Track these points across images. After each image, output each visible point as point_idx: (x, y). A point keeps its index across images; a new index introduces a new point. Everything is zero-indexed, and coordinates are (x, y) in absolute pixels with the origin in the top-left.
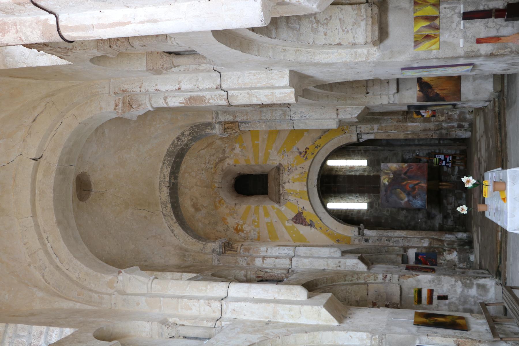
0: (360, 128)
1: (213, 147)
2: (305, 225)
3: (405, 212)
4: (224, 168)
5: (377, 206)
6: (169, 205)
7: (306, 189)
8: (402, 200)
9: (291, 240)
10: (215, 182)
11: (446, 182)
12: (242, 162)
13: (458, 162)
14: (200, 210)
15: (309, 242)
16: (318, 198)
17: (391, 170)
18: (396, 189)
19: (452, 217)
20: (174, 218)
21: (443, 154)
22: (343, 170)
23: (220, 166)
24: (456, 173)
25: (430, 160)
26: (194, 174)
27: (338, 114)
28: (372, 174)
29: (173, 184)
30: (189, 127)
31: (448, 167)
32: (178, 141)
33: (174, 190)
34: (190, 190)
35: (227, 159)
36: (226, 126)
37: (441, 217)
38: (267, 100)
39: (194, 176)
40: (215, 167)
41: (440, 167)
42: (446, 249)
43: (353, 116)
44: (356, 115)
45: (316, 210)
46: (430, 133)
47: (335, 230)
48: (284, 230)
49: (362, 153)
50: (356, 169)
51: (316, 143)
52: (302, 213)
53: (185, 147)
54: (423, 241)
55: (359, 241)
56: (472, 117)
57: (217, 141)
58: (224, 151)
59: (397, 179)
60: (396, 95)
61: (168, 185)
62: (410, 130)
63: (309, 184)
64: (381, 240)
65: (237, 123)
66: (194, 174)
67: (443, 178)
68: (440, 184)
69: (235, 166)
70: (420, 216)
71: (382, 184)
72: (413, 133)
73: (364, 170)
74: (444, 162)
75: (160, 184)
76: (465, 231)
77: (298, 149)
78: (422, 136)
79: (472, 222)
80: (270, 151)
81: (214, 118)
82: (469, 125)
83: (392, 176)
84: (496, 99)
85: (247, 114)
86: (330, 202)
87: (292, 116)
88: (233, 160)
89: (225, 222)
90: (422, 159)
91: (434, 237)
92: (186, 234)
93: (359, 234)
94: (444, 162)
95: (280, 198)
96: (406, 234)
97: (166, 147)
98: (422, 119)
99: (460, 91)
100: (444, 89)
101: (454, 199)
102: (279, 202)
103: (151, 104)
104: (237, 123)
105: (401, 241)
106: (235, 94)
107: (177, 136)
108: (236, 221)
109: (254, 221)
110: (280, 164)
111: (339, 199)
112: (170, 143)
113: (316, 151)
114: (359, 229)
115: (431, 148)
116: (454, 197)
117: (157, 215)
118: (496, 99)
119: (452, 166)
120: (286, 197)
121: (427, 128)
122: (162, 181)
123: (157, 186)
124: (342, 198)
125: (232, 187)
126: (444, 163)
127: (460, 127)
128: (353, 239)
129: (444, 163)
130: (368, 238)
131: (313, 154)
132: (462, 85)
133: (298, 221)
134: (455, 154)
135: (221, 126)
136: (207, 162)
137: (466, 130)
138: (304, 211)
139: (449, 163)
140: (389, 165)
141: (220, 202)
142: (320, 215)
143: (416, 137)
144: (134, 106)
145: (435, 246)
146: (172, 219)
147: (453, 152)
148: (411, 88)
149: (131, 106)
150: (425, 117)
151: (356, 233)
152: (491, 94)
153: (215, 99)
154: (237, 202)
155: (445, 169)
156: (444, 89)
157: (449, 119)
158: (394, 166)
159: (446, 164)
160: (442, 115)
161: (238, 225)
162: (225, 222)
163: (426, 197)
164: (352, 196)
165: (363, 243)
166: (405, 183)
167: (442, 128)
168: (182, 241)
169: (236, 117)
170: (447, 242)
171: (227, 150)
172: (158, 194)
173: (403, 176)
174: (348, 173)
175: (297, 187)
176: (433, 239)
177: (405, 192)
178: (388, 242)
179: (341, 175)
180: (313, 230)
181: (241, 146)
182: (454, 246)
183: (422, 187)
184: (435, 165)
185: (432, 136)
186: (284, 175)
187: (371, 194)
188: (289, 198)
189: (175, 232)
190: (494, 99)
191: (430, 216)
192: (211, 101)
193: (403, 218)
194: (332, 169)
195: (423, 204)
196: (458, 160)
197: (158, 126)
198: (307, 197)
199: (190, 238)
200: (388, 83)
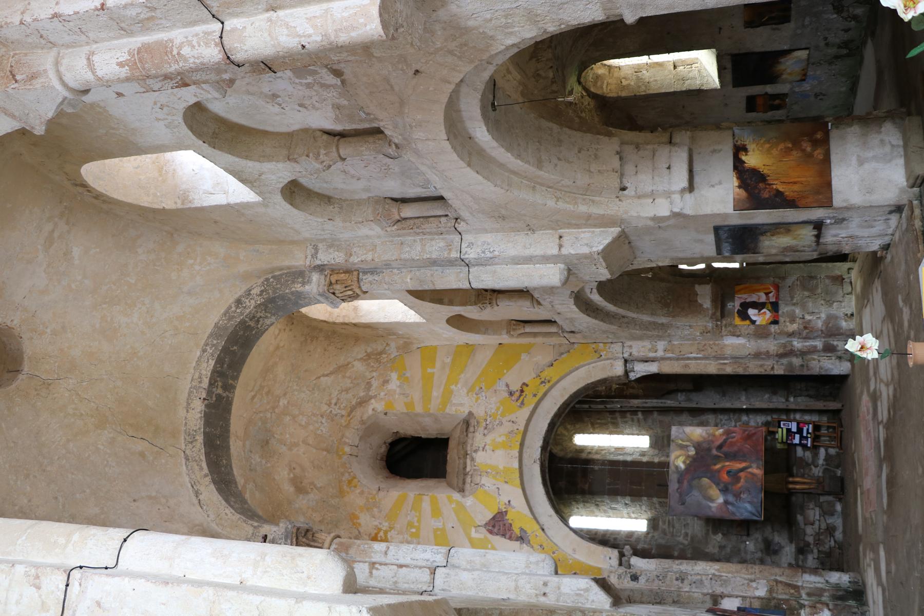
0: (631, 347)
1: (348, 374)
2: (510, 538)
4: (365, 417)
5: (666, 527)
6: (200, 438)
7: (516, 465)
8: (712, 501)
10: (345, 443)
11: (803, 476)
12: (400, 407)
14: (307, 493)
16: (541, 486)
17: (690, 440)
18: (700, 478)
19: (815, 551)
20: (204, 465)
23: (358, 413)
24: (821, 462)
26: (303, 420)
27: (560, 246)
29: (219, 397)
30: (262, 280)
31: (805, 447)
32: (237, 307)
33: (217, 412)
34: (290, 449)
35: (373, 401)
36: (334, 279)
37: (793, 550)
38: (311, 31)
39: (303, 423)
40: (349, 415)
42: (806, 603)
43: (595, 249)
44: (601, 247)
46: (769, 363)
47: (570, 551)
49: (638, 420)
51: (543, 375)
52: (506, 512)
53: (252, 324)
54: (754, 585)
55: (620, 577)
56: (852, 327)
57: (356, 363)
58: (369, 385)
59: (703, 459)
60: (687, 196)
61: (204, 395)
63: (525, 456)
64: (665, 577)
65: (355, 273)
66: (303, 420)
68: (791, 479)
69: (386, 414)
71: (672, 468)
72: (736, 359)
73: (643, 454)
74: (797, 436)
75: (190, 393)
77: (507, 385)
78: (754, 368)
80: (453, 387)
81: (309, 257)
83: (692, 452)
84: (915, 202)
85: (374, 248)
86: (576, 514)
87: (463, 251)
88: (383, 403)
89: (354, 524)
91: (779, 579)
92: (223, 502)
93: (620, 564)
94: (797, 436)
95: (464, 483)
96: (718, 570)
97: (214, 317)
98: (752, 327)
99: (829, 185)
100: (795, 183)
101: (817, 513)
102: (462, 490)
103: (58, 71)
104: (355, 273)
105: (707, 583)
106: (238, 26)
107: (236, 296)
108: (376, 523)
109: (410, 525)
110: (470, 413)
111: (593, 508)
112: (222, 311)
114: (622, 555)
116: (817, 509)
117: (171, 456)
118: (915, 202)
120: (477, 479)
121: (763, 350)
122: (195, 387)
123: (183, 397)
124: (597, 505)
125: (382, 459)
126: (797, 440)
129: (797, 440)
131: (535, 395)
132: (833, 174)
133: (495, 530)
135: (323, 277)
136: (334, 401)
138: (509, 509)
139: (807, 438)
140: (688, 429)
141: (350, 482)
142: (543, 520)
144: (18, 77)
145: (780, 597)
146: (201, 469)
148: (720, 183)
149: (14, 76)
150: (757, 323)
151: (615, 562)
152: (902, 191)
153: (195, 43)
154: (382, 486)
155: (799, 451)
156: (795, 183)
157: (805, 328)
158: (697, 432)
159: (801, 440)
160: (793, 321)
161: (380, 530)
162: (354, 524)
164: (618, 502)
166: (718, 466)
168: (212, 517)
169: (351, 255)
170: (808, 590)
171: (375, 384)
172: (182, 413)
173: (714, 452)
174: (612, 457)
175: (502, 466)
176: (777, 581)
177: (717, 484)
178: (679, 582)
179: (598, 460)
181: (401, 376)
182: (824, 599)
183: (753, 474)
184: (779, 446)
185: (773, 368)
186: (477, 434)
187: (655, 500)
188: (483, 482)
189: (201, 497)
190: (911, 202)
192: (186, 51)
193: (716, 550)
194: (581, 450)
197: (197, 268)
198: (518, 481)
199: (229, 511)
200: (669, 168)
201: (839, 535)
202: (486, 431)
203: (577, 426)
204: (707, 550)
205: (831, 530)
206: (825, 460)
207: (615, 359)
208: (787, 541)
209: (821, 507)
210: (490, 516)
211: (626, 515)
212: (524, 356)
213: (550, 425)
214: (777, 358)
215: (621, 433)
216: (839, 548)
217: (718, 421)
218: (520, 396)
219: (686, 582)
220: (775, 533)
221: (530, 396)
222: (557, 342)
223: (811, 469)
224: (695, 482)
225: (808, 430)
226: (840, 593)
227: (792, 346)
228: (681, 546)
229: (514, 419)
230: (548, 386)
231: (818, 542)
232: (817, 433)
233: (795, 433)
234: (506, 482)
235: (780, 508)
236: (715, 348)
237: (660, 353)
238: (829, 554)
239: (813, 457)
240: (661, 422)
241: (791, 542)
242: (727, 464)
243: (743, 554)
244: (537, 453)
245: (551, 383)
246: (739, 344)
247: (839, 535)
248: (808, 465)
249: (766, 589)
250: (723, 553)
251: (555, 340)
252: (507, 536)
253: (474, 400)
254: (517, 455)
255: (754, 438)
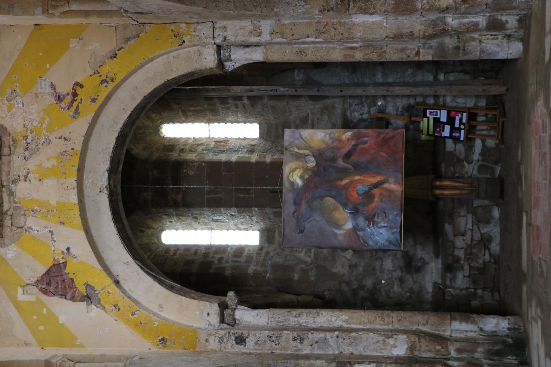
0: (224, 28)
2: (73, 299)
3: (349, 254)
7: (74, 198)
9: (32, 340)
11: (452, 178)
13: (482, 129)
15: (82, 346)
16: (112, 224)
17: (309, 148)
18: (322, 197)
19: (466, 267)
21: (444, 107)
22: (200, 148)
24: (476, 157)
25: (413, 122)
28: (268, 159)
31: (456, 140)
37: (440, 266)
41: (437, 141)
45: (105, 256)
47: (156, 310)
48: (13, 313)
49: (244, 106)
50: (231, 145)
51: (104, 71)
52: (65, 264)
54: (391, 341)
55: (221, 340)
59: (326, 172)
62: (359, 34)
63: (87, 183)
67: (443, 169)
68: (438, 183)
70: (388, 264)
71: (286, 184)
72: (368, 45)
73: (252, 149)
74: (447, 128)
76: (501, 311)
77: (53, 87)
78: (392, 54)
79: (524, 289)
82: (520, 21)
83: (312, 163)
86: (169, 228)
90: (393, 121)
93: (222, 321)
94: (447, 128)
101: (470, 221)
105: (332, 342)
111: (190, 221)
113: (105, 91)
114: (223, 307)
115: (415, 91)
116: (470, 216)
119: (467, 138)
120: (20, 221)
121: (406, 31)
124: (195, 218)
127: (495, 26)
128: (203, 337)
130: (245, 333)
133: (52, 289)
134: (475, 107)
137: (509, 37)
138: (69, 259)
139: (459, 129)
140: (306, 133)
142: (116, 269)
143: (375, 57)
145: (423, 355)
147: (470, 103)
151: (215, 319)
155: (450, 145)
158: (318, 137)
159: (451, 132)
163: (400, 219)
164: (221, 214)
165: (231, 346)
166: (345, 182)
167: (444, 32)
173: (341, 163)
174: (211, 157)
176: (420, 334)
177: (345, 205)
179: (193, 162)
180: (95, 310)
182: (477, 355)
183: (391, 192)
184: (424, 137)
185: (418, 53)
186: (14, 157)
187: (268, 210)
188: (29, 224)
191: (411, 265)
193: (345, 271)
194: (172, 145)
195: (392, 237)
196: (482, 123)
201: (495, 247)
202: (27, 153)
203: (165, 115)
204: (334, 270)
205: (485, 241)
206: (482, 154)
207: (204, 45)
208: (432, 255)
209: (474, 213)
210: (42, 270)
211: (234, 227)
212: (74, 44)
213: (118, 139)
214: (423, 41)
215: (223, 121)
216: (496, 263)
217: (347, 106)
218: (73, 101)
219: (306, 342)
220: (418, 247)
221: (87, 102)
222: (121, 23)
223: (463, 166)
224: (316, 203)
225: (461, 120)
226: (498, 347)
227: (445, 23)
228: (303, 266)
229: (67, 135)
230: (111, 86)
231: (470, 256)
232: (473, 123)
233: (444, 124)
234: (62, 223)
235: (424, 218)
236: (341, 29)
237: (265, 37)
238: (483, 270)
239: (466, 151)
240: (273, 107)
241: (437, 257)
242: (357, 178)
243: (378, 274)
244: (103, 180)
245: (116, 82)
246: (373, 22)
247: (495, 247)
248: (460, 161)
249: (406, 346)
250: (355, 273)
251: (115, 21)
252: (69, 296)
253: (6, 108)
254: (75, 184)
255: (392, 143)
